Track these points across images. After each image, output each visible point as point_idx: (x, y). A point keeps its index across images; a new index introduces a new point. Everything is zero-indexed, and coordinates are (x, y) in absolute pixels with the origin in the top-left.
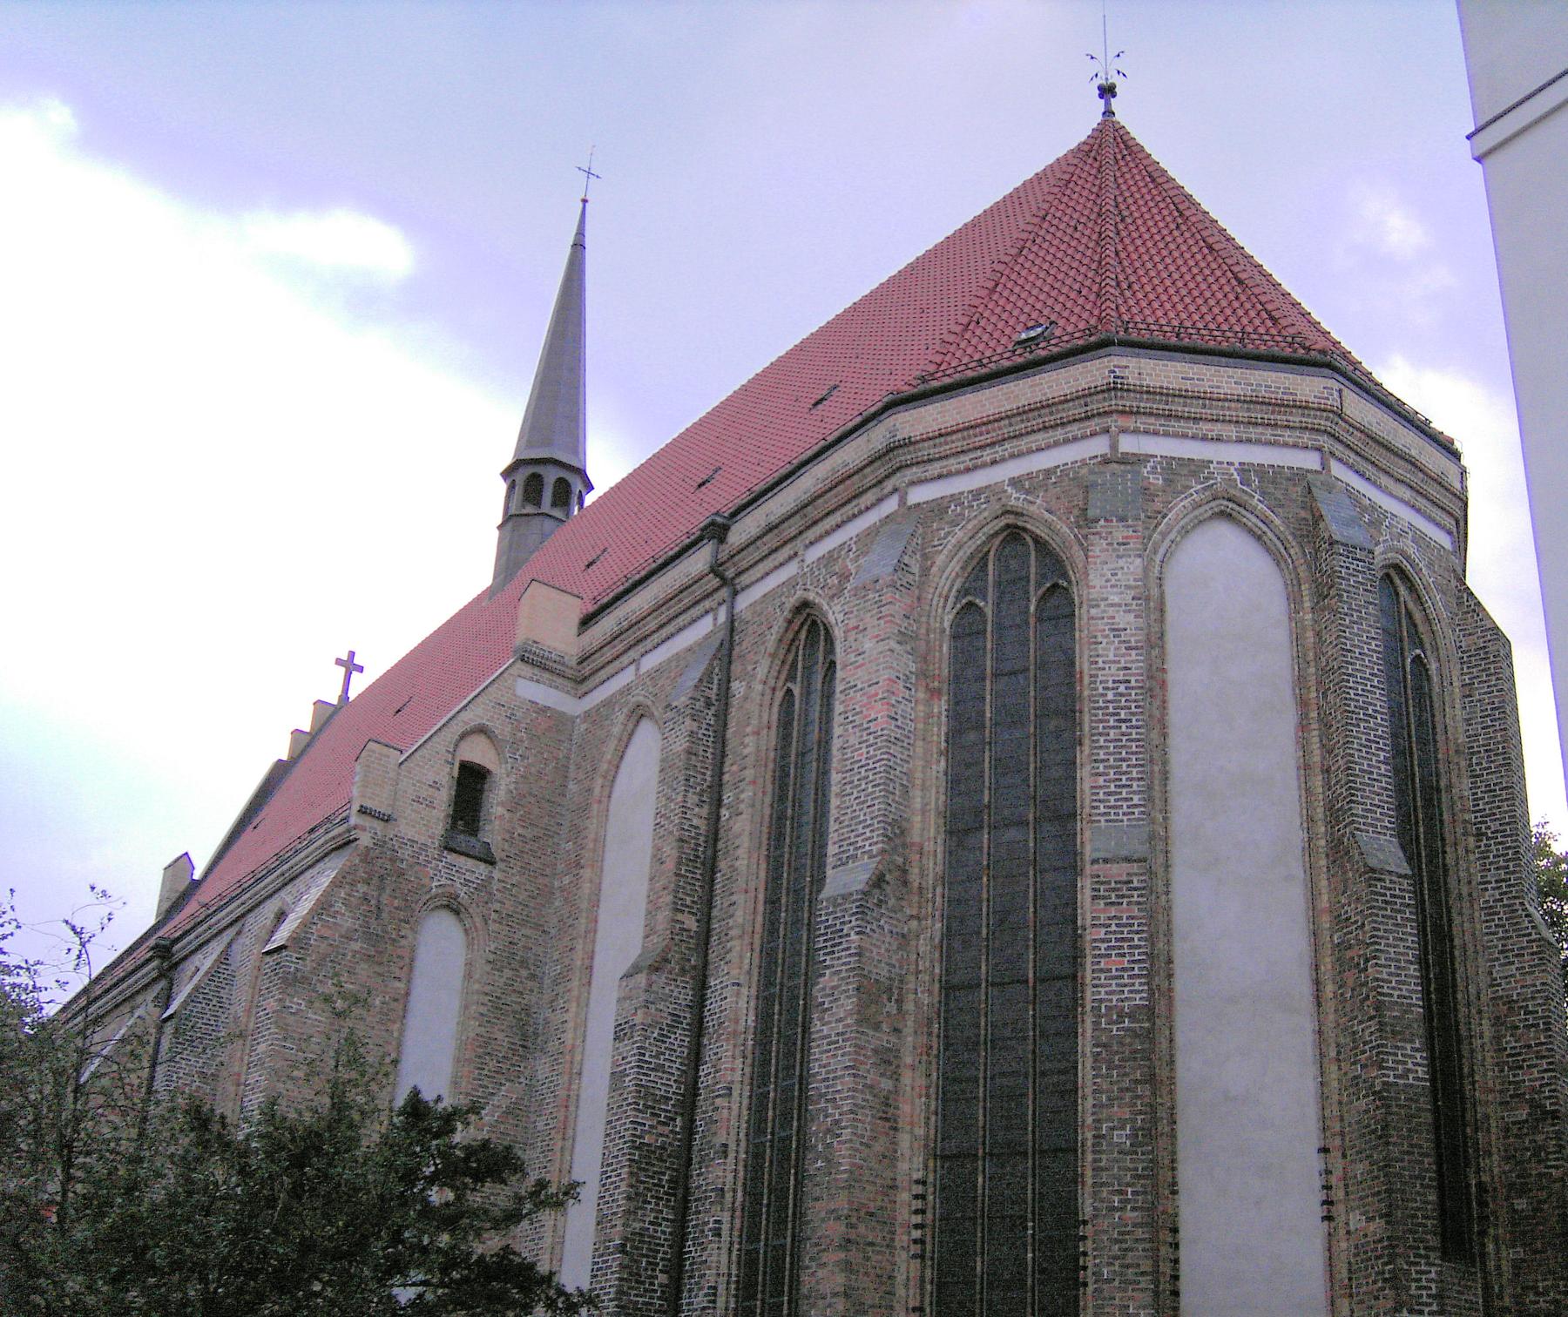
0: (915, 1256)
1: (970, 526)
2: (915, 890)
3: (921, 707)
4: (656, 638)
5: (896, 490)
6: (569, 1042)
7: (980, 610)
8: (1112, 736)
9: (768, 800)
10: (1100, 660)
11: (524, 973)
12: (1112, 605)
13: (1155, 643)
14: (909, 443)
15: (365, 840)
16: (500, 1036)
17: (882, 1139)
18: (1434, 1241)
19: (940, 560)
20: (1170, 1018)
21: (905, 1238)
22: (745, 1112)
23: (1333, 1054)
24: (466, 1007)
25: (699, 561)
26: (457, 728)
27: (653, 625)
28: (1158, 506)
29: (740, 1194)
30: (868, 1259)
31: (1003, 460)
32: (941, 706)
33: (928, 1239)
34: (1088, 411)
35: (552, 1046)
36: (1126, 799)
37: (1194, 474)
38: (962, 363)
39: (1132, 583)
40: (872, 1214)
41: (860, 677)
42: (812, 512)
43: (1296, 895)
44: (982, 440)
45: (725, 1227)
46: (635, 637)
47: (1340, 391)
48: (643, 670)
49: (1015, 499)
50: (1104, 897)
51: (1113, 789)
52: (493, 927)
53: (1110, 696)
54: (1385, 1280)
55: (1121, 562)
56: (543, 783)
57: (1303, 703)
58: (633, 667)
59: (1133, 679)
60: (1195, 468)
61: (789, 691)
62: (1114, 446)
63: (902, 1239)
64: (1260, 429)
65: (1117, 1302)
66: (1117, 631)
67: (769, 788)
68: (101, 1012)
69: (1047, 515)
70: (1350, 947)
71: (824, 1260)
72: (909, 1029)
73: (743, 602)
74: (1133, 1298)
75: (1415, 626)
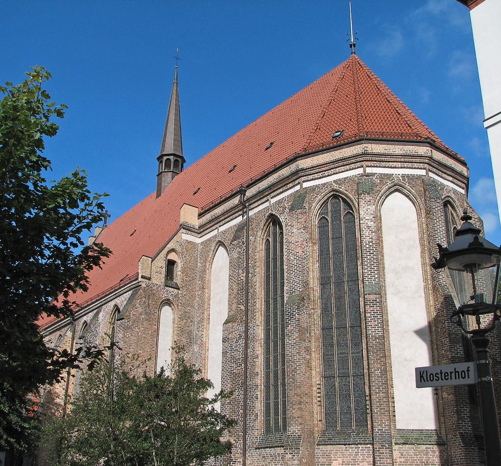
0: (319, 406)
1: (322, 195)
2: (312, 301)
3: (311, 248)
4: (224, 222)
5: (299, 183)
6: (204, 341)
7: (327, 219)
8: (368, 258)
9: (263, 272)
10: (364, 236)
11: (189, 320)
12: (367, 220)
13: (379, 229)
14: (303, 170)
15: (144, 285)
16: (184, 339)
17: (308, 373)
18: (468, 401)
19: (314, 205)
20: (388, 338)
21: (316, 400)
22: (263, 363)
23: (436, 347)
24: (174, 332)
25: (236, 201)
26: (166, 250)
27: (223, 218)
28: (378, 188)
29: (263, 386)
30: (306, 407)
31: (331, 175)
32: (316, 247)
33: (322, 401)
35: (199, 342)
36: (374, 276)
37: (388, 178)
38: (317, 142)
39: (372, 213)
40: (307, 394)
41: (293, 240)
43: (422, 301)
44: (324, 169)
45: (259, 396)
46: (217, 221)
47: (432, 150)
48: (219, 231)
49: (336, 187)
50: (369, 305)
51: (369, 273)
52: (180, 307)
53: (367, 246)
54: (454, 412)
55: (369, 207)
56: (191, 264)
57: (422, 245)
58: (217, 230)
59: (374, 241)
60: (389, 176)
61: (268, 240)
62: (365, 171)
63: (315, 401)
64: (408, 164)
65: (379, 419)
66: (369, 227)
67: (263, 268)
69: (345, 192)
70: (440, 317)
71: (294, 407)
72: (313, 341)
74: (383, 418)
75: (454, 218)
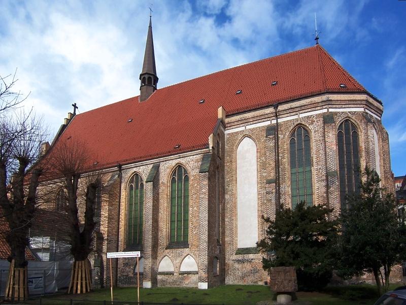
34: (329, 102)
42: (303, 108)
68: (125, 168)
73: (279, 120)
